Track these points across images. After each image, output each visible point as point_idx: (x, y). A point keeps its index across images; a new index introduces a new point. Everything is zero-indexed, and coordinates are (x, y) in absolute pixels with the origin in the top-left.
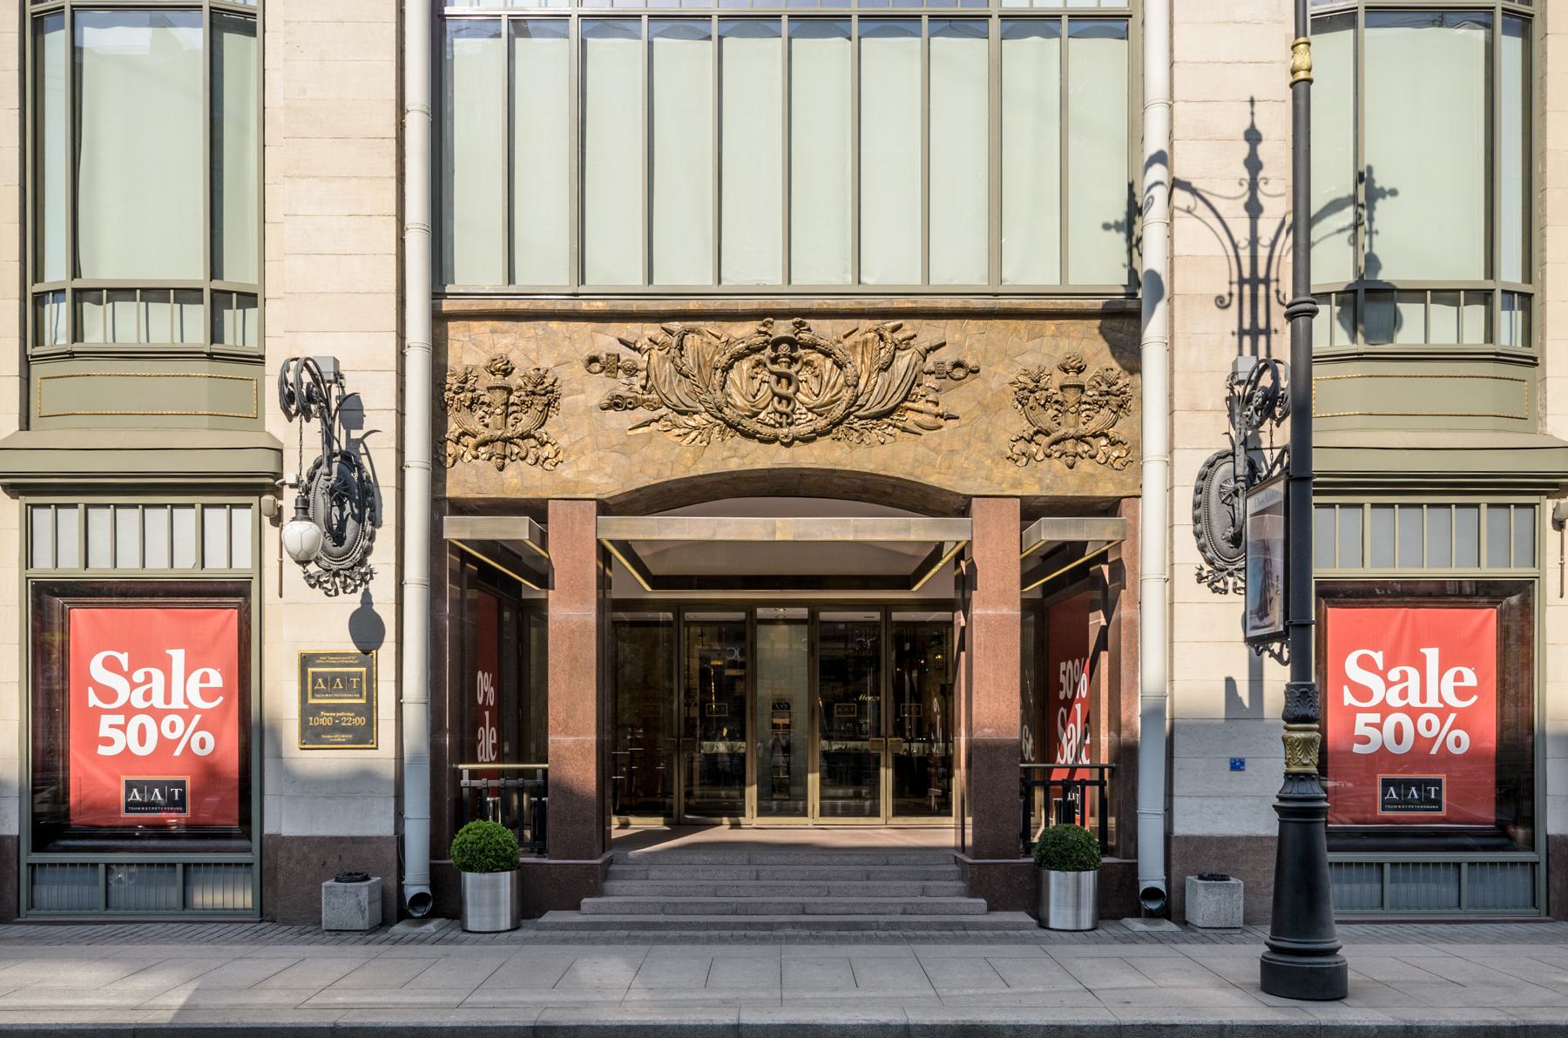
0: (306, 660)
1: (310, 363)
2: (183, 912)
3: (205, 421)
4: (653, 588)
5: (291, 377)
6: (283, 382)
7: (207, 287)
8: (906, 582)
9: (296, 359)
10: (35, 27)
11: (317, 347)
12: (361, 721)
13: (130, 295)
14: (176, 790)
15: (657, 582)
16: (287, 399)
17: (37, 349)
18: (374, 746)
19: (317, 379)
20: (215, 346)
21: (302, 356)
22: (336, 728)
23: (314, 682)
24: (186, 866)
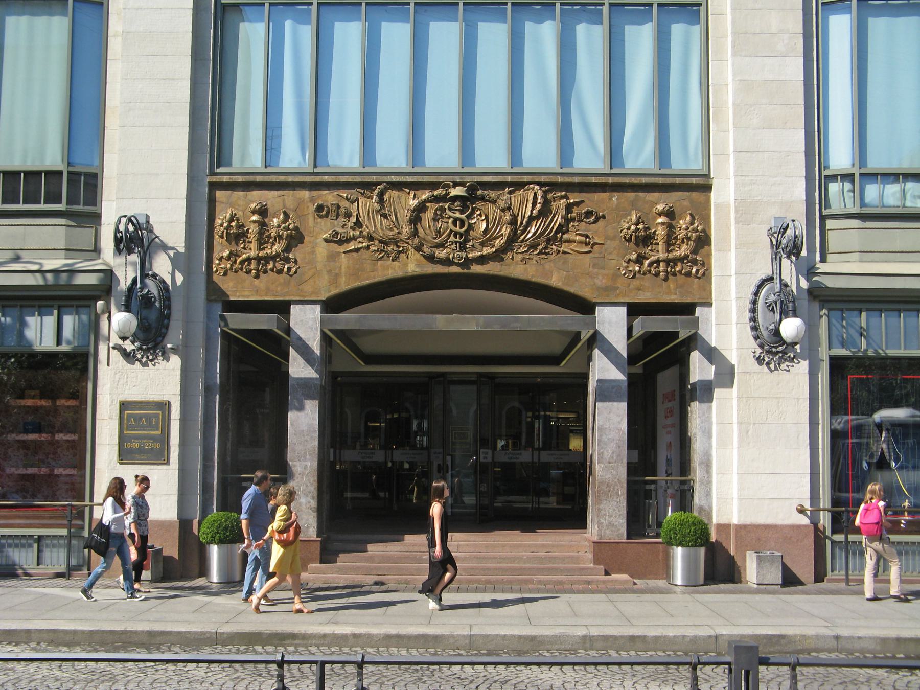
0: (124, 406)
1: (133, 218)
2: (38, 567)
3: (856, 256)
4: (366, 364)
5: (122, 228)
6: (117, 230)
7: (856, 171)
8: (556, 360)
9: (125, 216)
10: (223, 10)
11: (136, 209)
12: (157, 446)
13: (875, 177)
14: (348, 495)
15: (369, 359)
16: (118, 241)
17: (827, 210)
18: (166, 462)
19: (138, 227)
20: (863, 209)
21: (129, 215)
22: (141, 451)
23: (157, 423)
24: (40, 538)
